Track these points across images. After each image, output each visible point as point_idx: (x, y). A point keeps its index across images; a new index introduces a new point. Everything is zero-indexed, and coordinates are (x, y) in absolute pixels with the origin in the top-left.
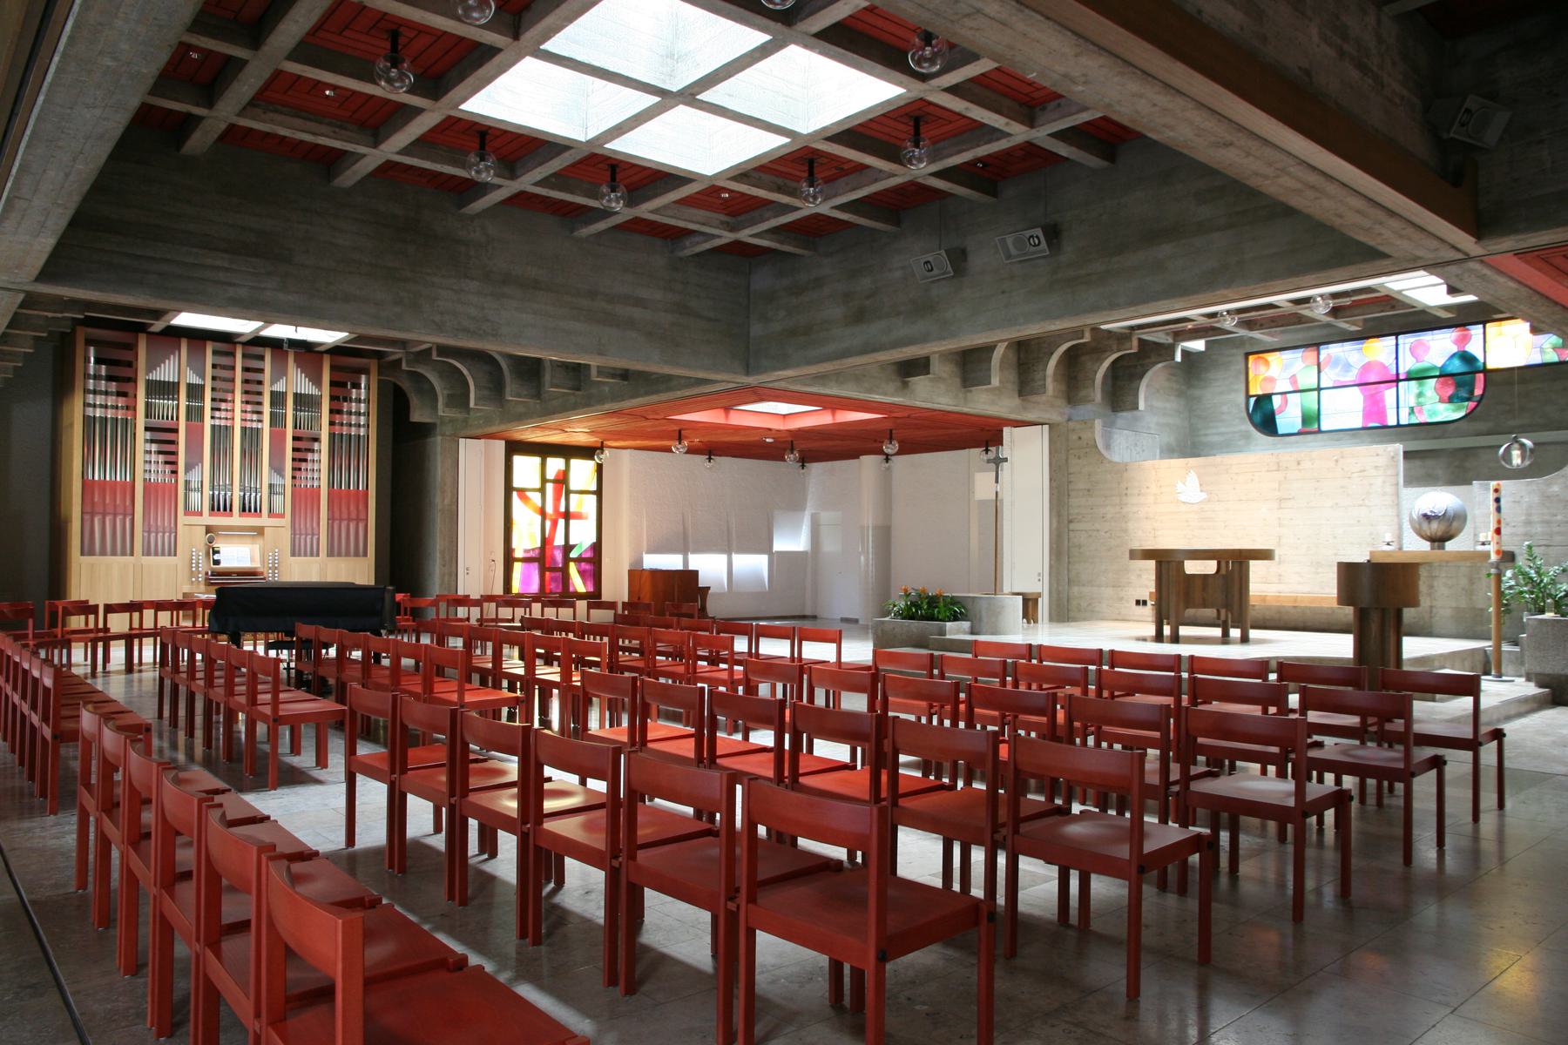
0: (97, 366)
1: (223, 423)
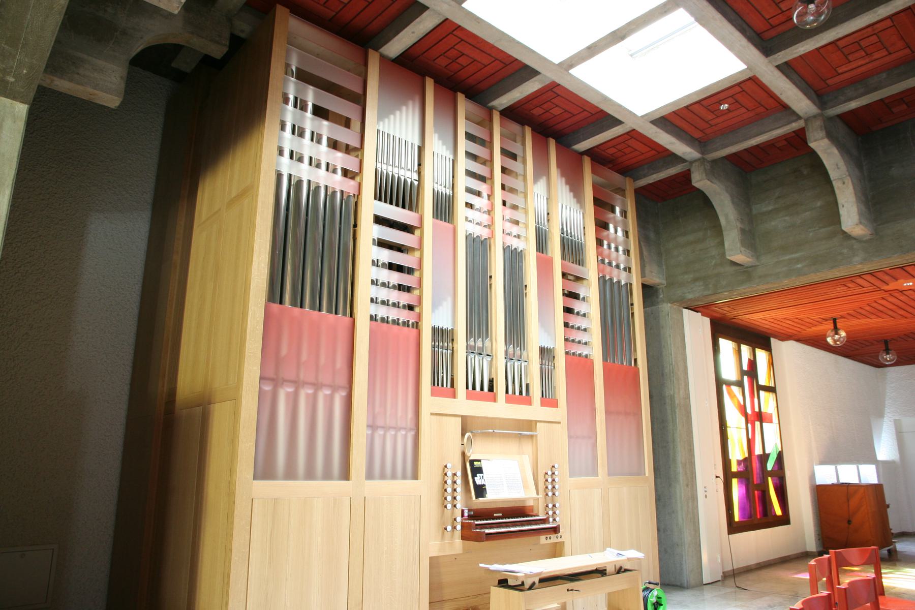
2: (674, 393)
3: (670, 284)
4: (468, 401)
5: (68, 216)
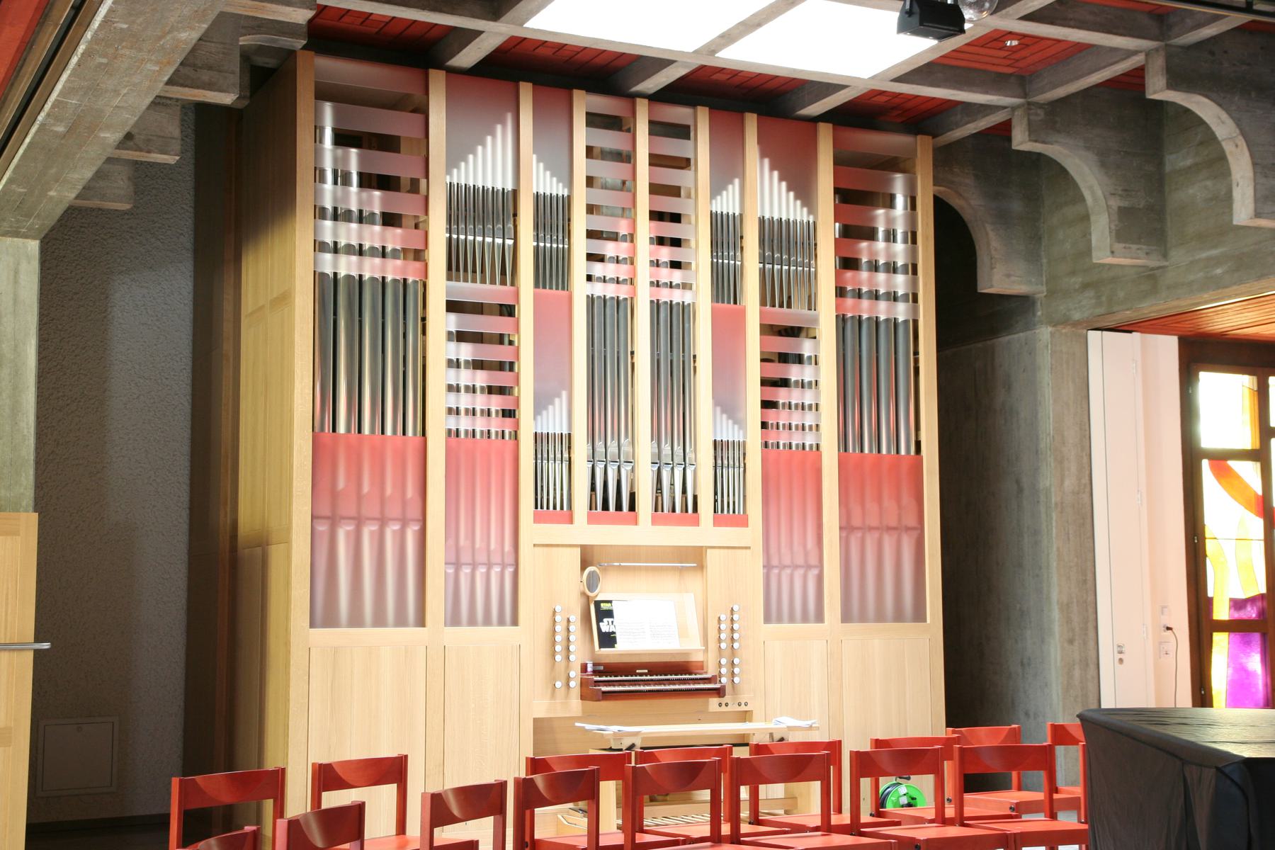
0: (340, 151)
1: (610, 291)
2: (1050, 485)
3: (1051, 293)
4: (591, 526)
5: (84, 285)
